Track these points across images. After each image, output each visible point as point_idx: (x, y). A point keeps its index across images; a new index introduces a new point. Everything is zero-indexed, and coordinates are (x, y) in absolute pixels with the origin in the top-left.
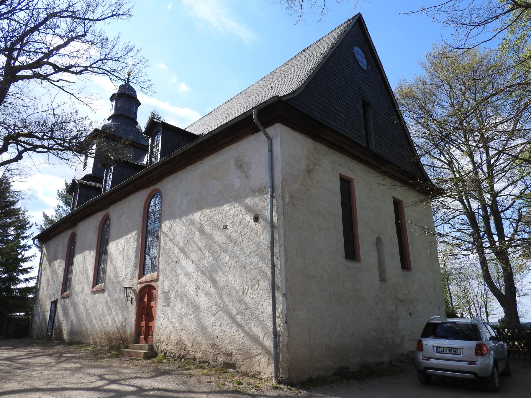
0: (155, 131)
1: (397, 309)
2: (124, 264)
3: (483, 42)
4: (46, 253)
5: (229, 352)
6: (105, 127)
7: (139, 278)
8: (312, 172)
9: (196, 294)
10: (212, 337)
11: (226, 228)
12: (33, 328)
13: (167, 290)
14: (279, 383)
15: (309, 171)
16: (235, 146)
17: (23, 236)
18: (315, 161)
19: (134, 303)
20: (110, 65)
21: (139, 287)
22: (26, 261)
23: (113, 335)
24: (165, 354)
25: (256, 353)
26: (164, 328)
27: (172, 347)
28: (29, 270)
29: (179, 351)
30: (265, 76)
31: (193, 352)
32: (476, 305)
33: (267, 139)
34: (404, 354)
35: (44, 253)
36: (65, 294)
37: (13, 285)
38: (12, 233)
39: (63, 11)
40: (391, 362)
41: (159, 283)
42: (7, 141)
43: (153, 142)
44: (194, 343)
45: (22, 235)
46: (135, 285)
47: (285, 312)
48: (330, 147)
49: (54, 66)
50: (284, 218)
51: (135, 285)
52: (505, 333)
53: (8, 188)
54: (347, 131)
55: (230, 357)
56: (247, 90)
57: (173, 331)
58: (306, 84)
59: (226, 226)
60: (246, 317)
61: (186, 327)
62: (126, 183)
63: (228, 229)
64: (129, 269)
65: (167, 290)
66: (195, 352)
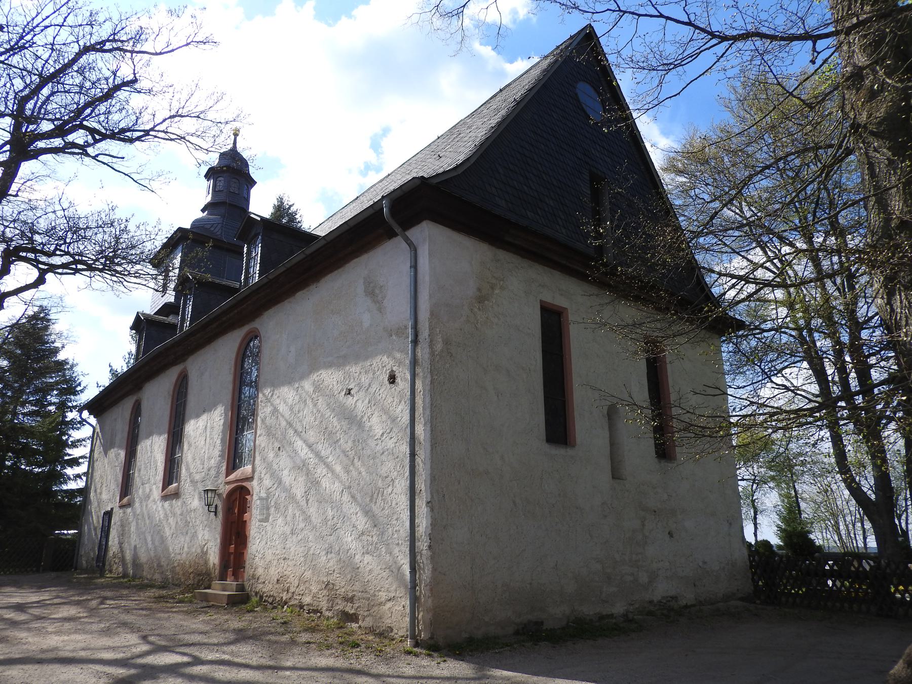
0: (253, 233)
1: (643, 525)
2: (206, 452)
3: (667, 98)
4: (100, 434)
5: (350, 595)
6: (196, 224)
7: (227, 475)
8: (488, 300)
9: (305, 502)
10: (327, 570)
11: (349, 393)
12: (81, 556)
13: (266, 495)
14: (417, 645)
15: (482, 299)
16: (364, 258)
17: (71, 405)
18: (494, 281)
19: (220, 515)
20: (186, 126)
21: (229, 488)
22: (76, 446)
23: (190, 567)
24: (261, 597)
25: (387, 597)
26: (260, 556)
27: (271, 586)
28: (81, 460)
29: (280, 593)
30: (442, 134)
31: (300, 594)
32: (848, 518)
33: (409, 248)
34: (655, 601)
35: (98, 432)
36: (125, 500)
37: (55, 485)
38: (54, 400)
39: (103, 43)
40: (625, 615)
41: (255, 483)
42: (13, 255)
43: (249, 252)
44: (302, 581)
45: (70, 404)
46: (221, 486)
47: (429, 531)
48: (523, 257)
49: (92, 131)
50: (432, 377)
51: (221, 486)
52: (854, 567)
53: (46, 328)
54: (558, 227)
55: (351, 603)
56: (413, 159)
57: (272, 562)
58: (479, 153)
59: (350, 390)
60: (374, 539)
61: (291, 555)
62: (208, 320)
63: (353, 396)
64: (213, 461)
65: (266, 495)
66: (302, 595)
